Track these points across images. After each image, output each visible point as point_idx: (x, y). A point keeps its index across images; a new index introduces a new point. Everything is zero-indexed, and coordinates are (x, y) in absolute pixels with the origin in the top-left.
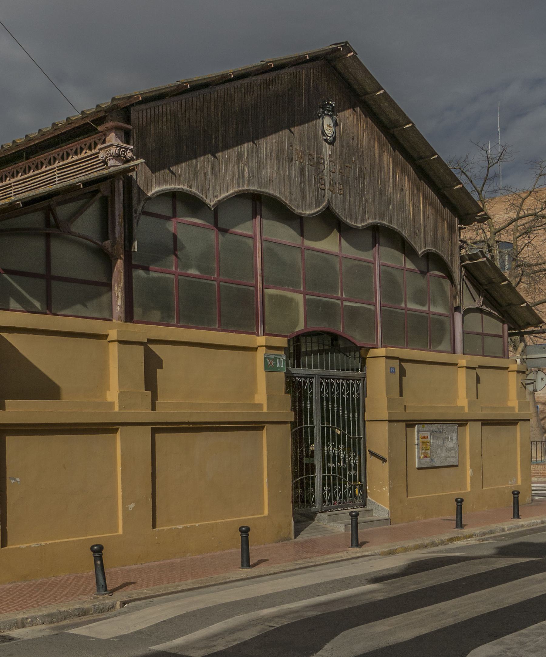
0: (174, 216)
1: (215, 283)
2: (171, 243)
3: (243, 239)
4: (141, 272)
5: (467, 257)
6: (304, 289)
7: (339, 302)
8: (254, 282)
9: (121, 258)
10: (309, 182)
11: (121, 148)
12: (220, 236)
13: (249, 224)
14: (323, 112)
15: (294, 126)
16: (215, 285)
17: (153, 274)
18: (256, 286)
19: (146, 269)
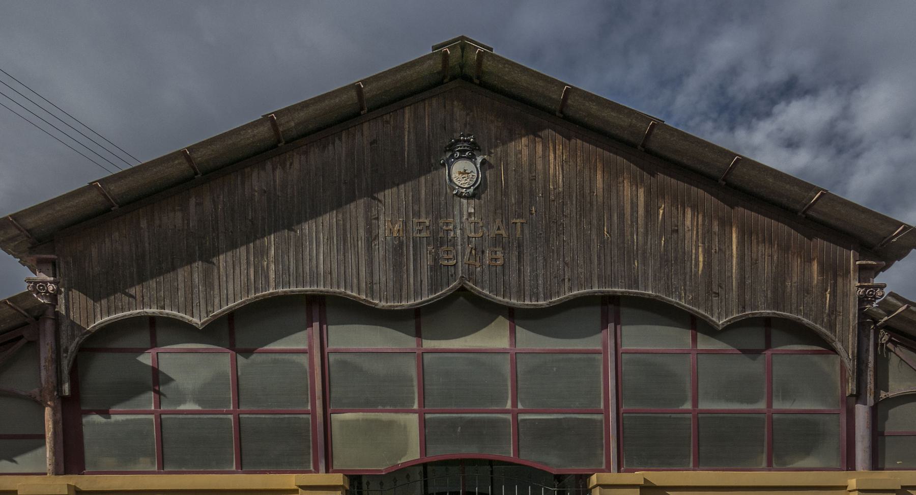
0: (768, 346)
1: (231, 417)
2: (150, 378)
3: (294, 357)
4: (97, 418)
5: (880, 311)
6: (419, 405)
7: (509, 417)
8: (309, 408)
9: (49, 406)
10: (415, 260)
11: (36, 283)
12: (241, 359)
13: (599, 337)
14: (452, 156)
15: (384, 189)
16: (230, 419)
17: (115, 418)
18: (313, 413)
19: (105, 413)
